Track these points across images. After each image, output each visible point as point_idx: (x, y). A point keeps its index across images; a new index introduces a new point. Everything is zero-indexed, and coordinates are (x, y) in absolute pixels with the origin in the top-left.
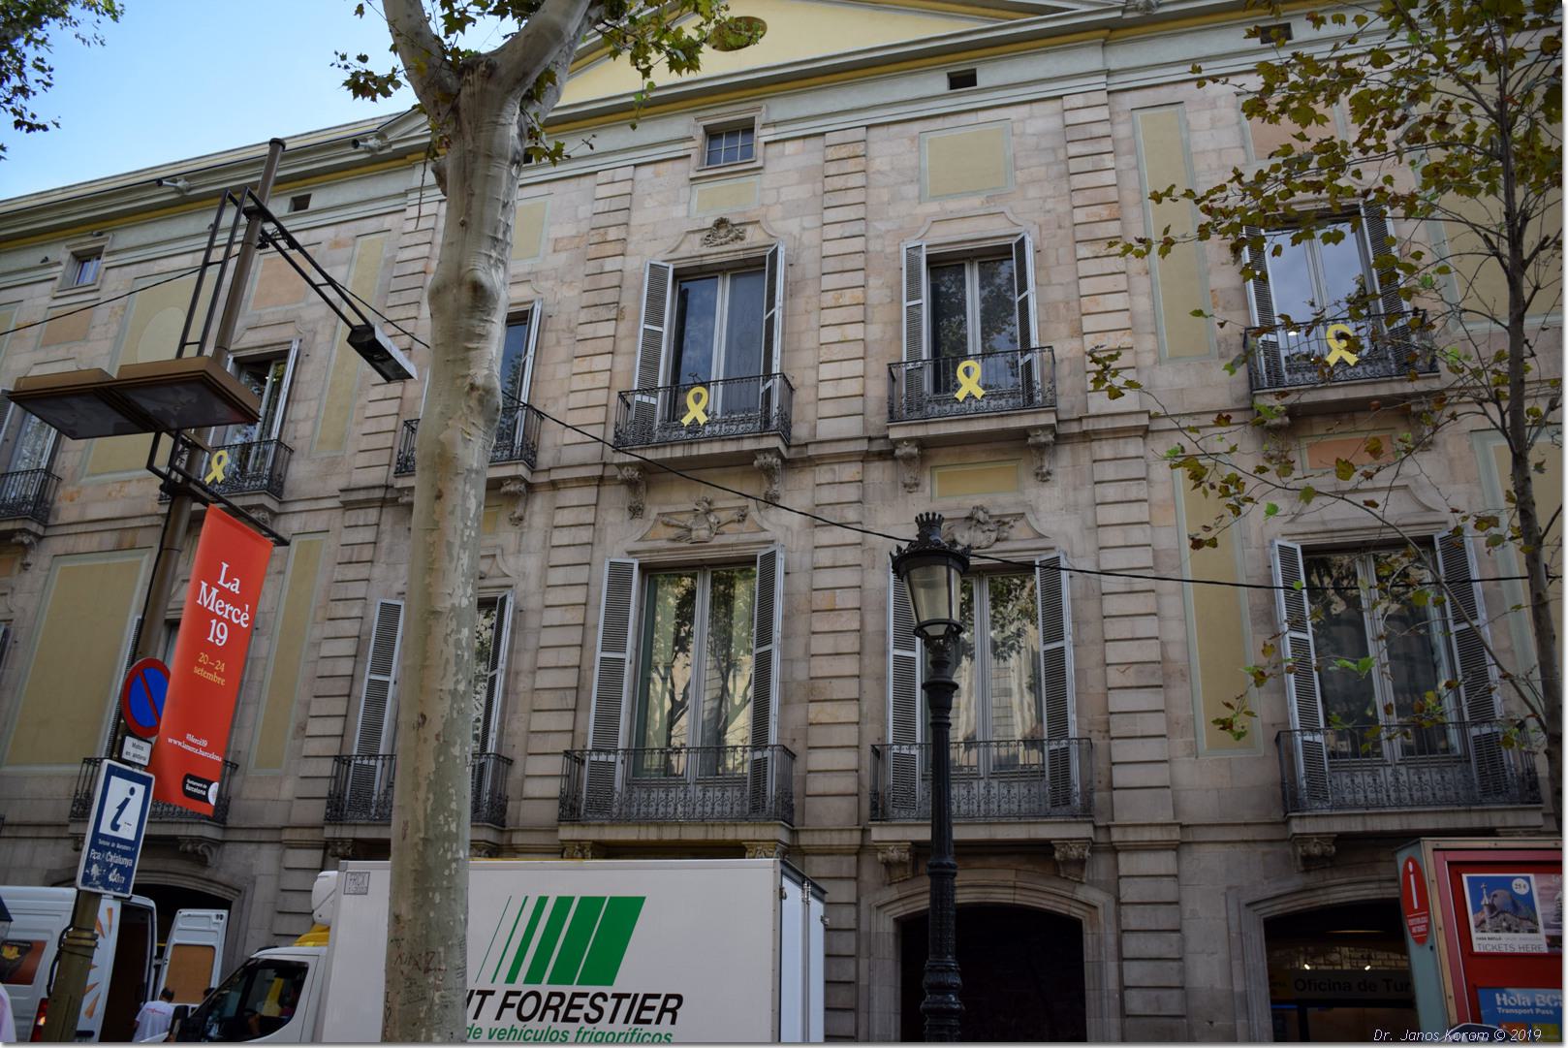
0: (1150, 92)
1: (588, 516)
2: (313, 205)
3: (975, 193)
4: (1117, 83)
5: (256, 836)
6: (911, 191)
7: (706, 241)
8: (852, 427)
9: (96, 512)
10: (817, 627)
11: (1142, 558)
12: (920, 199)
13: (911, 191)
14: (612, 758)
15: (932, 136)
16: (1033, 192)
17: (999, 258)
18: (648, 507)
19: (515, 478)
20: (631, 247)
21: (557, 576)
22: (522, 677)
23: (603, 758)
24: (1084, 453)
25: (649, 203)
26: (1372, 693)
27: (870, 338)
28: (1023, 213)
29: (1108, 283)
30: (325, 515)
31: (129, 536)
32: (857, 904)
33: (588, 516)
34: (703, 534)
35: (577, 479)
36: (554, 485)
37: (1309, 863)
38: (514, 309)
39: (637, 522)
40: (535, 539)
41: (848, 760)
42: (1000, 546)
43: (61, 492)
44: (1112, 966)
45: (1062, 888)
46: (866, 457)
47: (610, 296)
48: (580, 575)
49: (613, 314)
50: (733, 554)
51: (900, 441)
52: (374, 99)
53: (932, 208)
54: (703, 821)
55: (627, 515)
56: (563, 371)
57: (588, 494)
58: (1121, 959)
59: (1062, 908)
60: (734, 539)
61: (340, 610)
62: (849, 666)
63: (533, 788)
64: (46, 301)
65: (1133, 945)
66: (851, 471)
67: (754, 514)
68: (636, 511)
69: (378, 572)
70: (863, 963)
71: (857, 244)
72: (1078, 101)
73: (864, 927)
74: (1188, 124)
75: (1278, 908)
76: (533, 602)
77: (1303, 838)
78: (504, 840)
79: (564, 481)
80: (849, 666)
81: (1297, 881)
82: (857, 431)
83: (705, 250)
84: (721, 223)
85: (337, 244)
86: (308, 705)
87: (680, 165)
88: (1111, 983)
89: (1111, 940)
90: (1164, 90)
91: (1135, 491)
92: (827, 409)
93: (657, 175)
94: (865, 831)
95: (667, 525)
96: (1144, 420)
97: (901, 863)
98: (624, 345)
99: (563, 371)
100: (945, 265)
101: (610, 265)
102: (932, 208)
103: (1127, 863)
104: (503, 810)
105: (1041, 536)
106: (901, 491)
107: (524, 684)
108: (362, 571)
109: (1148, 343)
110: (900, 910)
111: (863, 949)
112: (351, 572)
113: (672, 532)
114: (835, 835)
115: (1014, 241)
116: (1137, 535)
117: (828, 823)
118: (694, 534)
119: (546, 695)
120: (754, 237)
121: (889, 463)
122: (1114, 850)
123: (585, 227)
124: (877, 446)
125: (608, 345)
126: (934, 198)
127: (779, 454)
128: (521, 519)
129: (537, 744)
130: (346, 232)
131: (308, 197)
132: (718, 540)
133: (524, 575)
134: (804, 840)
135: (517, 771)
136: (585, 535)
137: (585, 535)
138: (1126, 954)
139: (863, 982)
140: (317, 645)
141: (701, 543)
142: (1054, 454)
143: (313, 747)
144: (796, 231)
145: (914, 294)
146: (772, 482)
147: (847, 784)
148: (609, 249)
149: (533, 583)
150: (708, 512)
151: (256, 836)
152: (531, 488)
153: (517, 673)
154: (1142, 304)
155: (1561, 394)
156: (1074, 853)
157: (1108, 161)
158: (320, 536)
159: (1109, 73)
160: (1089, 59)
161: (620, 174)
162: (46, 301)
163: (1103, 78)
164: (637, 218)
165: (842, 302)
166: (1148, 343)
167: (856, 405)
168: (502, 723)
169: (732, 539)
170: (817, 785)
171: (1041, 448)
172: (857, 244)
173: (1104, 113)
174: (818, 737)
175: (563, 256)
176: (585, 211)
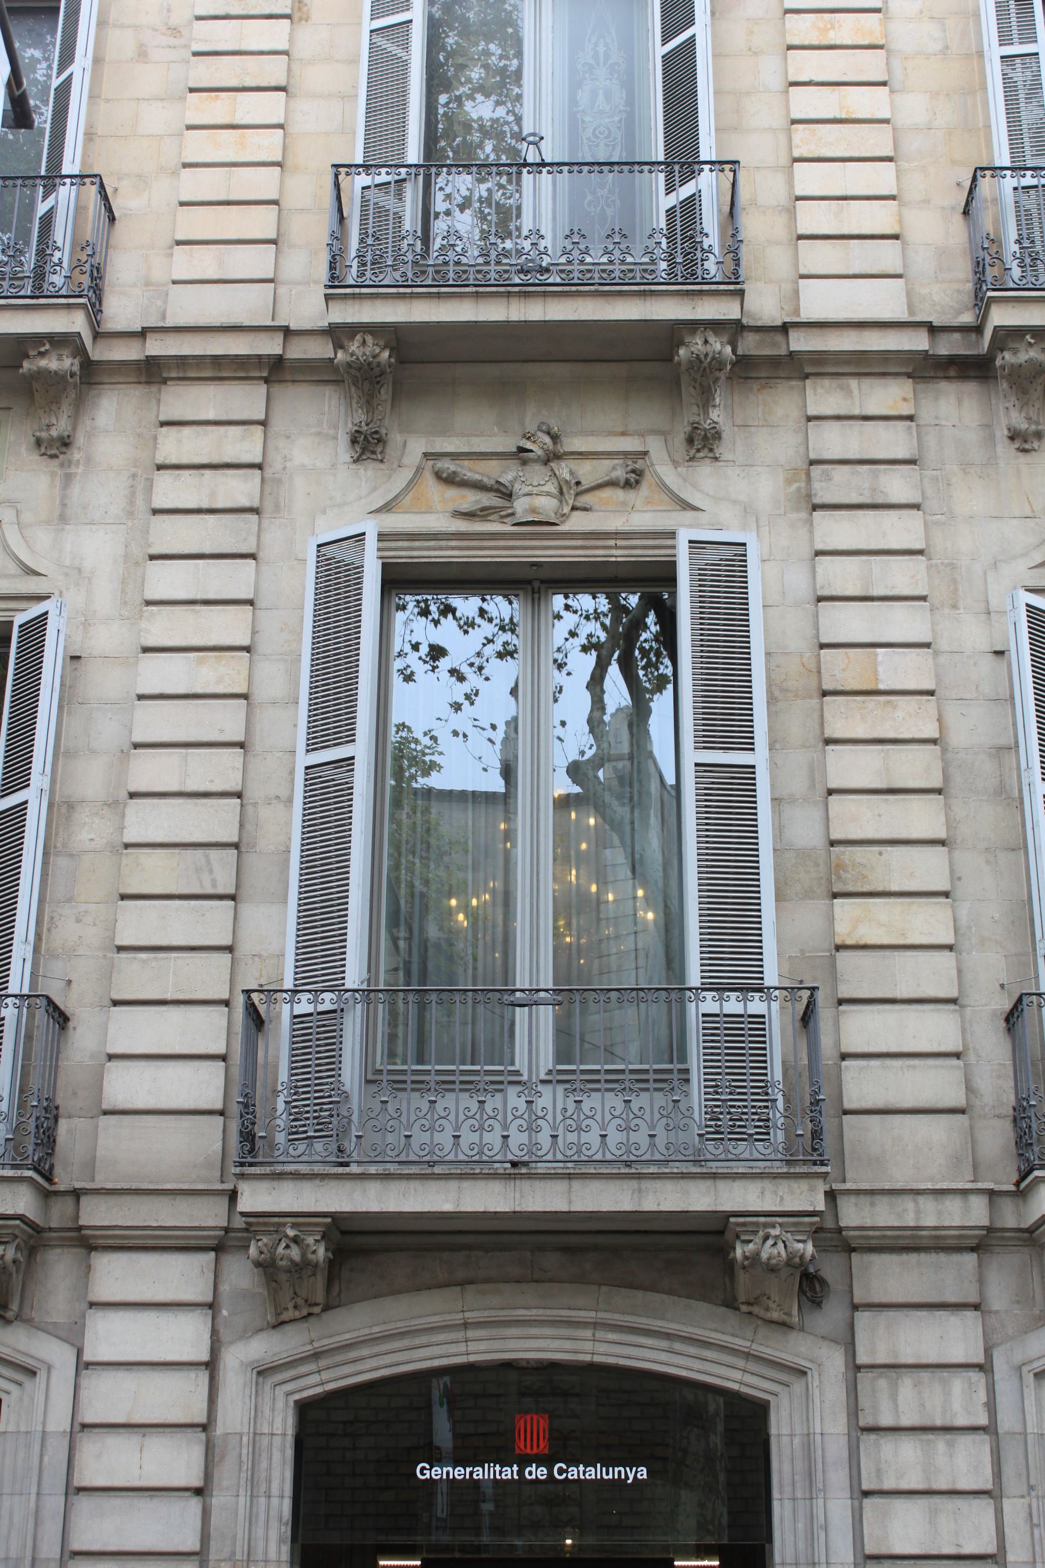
1: (245, 446)
10: (837, 729)
14: (756, 1006)
18: (396, 438)
19: (59, 341)
22: (82, 815)
23: (733, 1005)
24: (782, 404)
26: (303, 925)
27: (903, 119)
32: (211, 1365)
33: (245, 446)
34: (547, 505)
35: (217, 361)
36: (153, 372)
39: (369, 471)
44: (838, 1507)
46: (925, 369)
50: (618, 555)
51: (1017, 333)
55: (344, 452)
56: (158, 118)
60: (619, 520)
65: (177, 1462)
66: (888, 395)
67: (664, 469)
68: (367, 445)
70: (1013, 1508)
73: (1007, 1421)
76: (108, 638)
78: (58, 1215)
79: (182, 361)
82: (896, 311)
89: (836, 1448)
94: (233, 1196)
95: (450, 480)
97: (302, 1268)
98: (315, 78)
99: (158, 118)
103: (116, 1275)
104: (48, 1140)
106: (1005, 449)
107: (90, 832)
111: (1009, 1471)
113: (470, 499)
114: (928, 1204)
117: (900, 1177)
118: (520, 505)
121: (970, 388)
124: (947, 347)
127: (80, 351)
128: (65, 443)
129: (138, 977)
132: (578, 522)
133: (78, 573)
134: (853, 1215)
135: (84, 1041)
136: (239, 489)
137: (239, 489)
141: (539, 526)
142: (79, 406)
146: (706, 401)
149: (104, 595)
150: (551, 457)
152: (92, 374)
153: (71, 806)
170: (125, 1086)
171: (705, 378)
174: (858, 975)
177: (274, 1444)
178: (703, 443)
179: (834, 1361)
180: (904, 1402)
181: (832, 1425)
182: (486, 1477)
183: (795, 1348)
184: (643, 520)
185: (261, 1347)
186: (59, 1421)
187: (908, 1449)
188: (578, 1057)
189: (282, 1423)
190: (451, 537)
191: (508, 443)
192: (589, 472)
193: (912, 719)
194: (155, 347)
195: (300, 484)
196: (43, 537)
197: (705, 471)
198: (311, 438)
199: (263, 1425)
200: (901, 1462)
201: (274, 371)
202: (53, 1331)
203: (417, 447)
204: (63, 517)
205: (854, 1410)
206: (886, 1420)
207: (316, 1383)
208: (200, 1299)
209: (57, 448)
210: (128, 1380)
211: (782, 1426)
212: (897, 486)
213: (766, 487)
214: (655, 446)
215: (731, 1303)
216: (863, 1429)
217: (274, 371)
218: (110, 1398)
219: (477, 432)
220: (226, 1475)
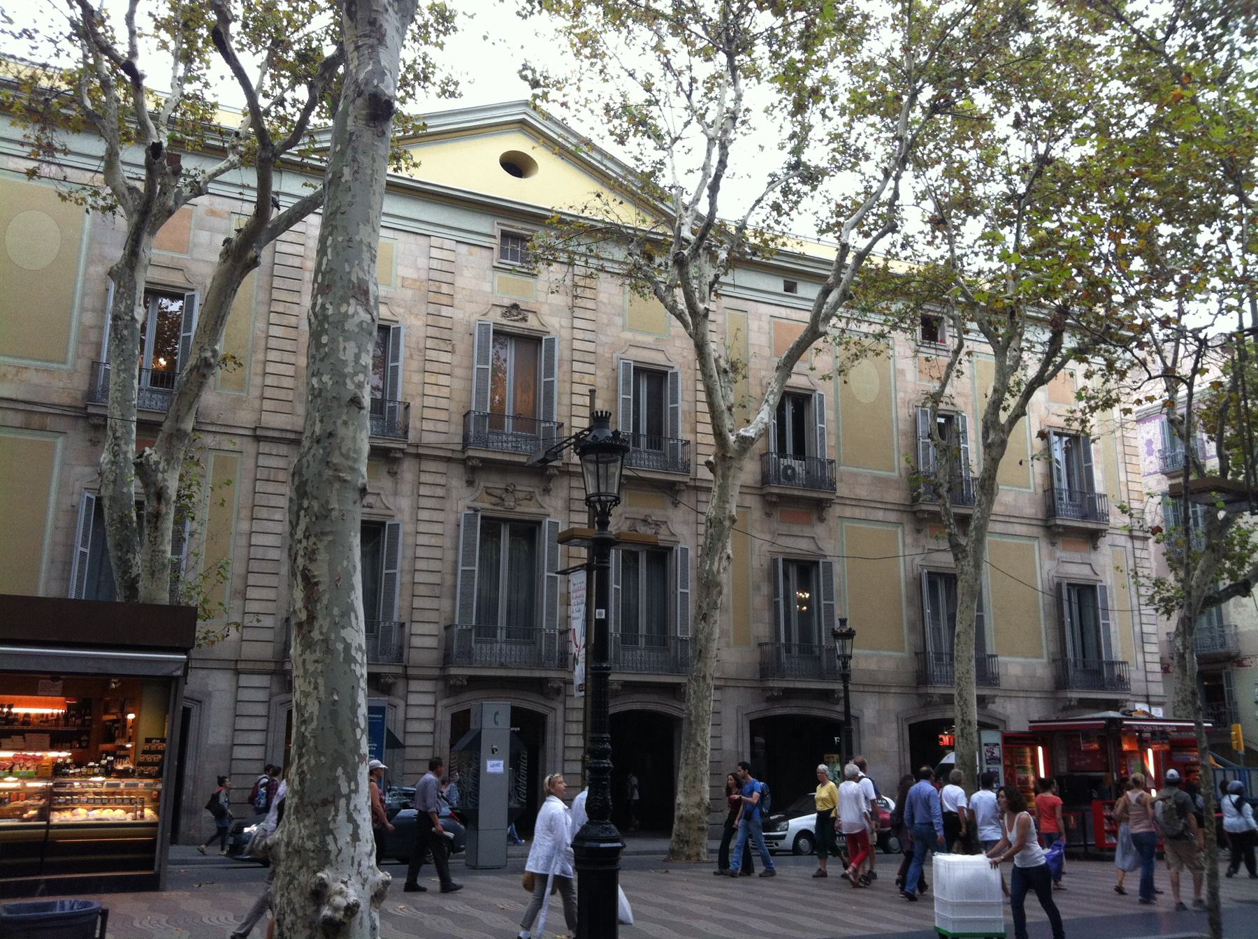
3: (650, 333)
5: (210, 664)
6: (619, 321)
7: (504, 315)
12: (624, 328)
13: (619, 321)
16: (678, 343)
24: (565, 482)
25: (466, 273)
30: (237, 440)
31: (36, 420)
32: (435, 706)
37: (769, 699)
39: (471, 489)
40: (406, 488)
44: (560, 738)
45: (677, 704)
52: (731, 141)
53: (628, 335)
54: (502, 666)
60: (528, 510)
61: (264, 513)
68: (470, 483)
75: (754, 717)
77: (772, 689)
81: (763, 706)
83: (504, 322)
84: (515, 306)
87: (485, 253)
89: (560, 725)
93: (471, 254)
101: (445, 311)
102: (628, 335)
103: (414, 685)
105: (673, 535)
113: (494, 500)
119: (422, 587)
120: (532, 323)
122: (407, 678)
123: (424, 276)
126: (631, 330)
132: (518, 509)
133: (400, 510)
136: (440, 492)
137: (440, 492)
141: (511, 510)
144: (557, 326)
148: (445, 300)
151: (210, 664)
155: (52, 468)
156: (555, 685)
158: (235, 455)
169: (526, 510)
174: (417, 616)
175: (409, 293)
176: (423, 262)
178: (547, 491)
179: (561, 707)
181: (560, 720)
182: (385, 221)
183: (554, 704)
184: (533, 510)
185: (445, 702)
188: (993, 850)
189: (449, 718)
191: (502, 486)
192: (521, 495)
194: (421, 451)
195: (454, 491)
196: (391, 499)
197: (547, 498)
198: (456, 482)
199: (445, 718)
201: (448, 460)
202: (400, 697)
204: (395, 494)
207: (456, 709)
209: (393, 474)
210: (418, 709)
211: (550, 719)
213: (559, 503)
214: (536, 491)
215: (542, 694)
216: (566, 721)
217: (448, 460)
218: (413, 713)
219: (496, 482)
220: (438, 730)
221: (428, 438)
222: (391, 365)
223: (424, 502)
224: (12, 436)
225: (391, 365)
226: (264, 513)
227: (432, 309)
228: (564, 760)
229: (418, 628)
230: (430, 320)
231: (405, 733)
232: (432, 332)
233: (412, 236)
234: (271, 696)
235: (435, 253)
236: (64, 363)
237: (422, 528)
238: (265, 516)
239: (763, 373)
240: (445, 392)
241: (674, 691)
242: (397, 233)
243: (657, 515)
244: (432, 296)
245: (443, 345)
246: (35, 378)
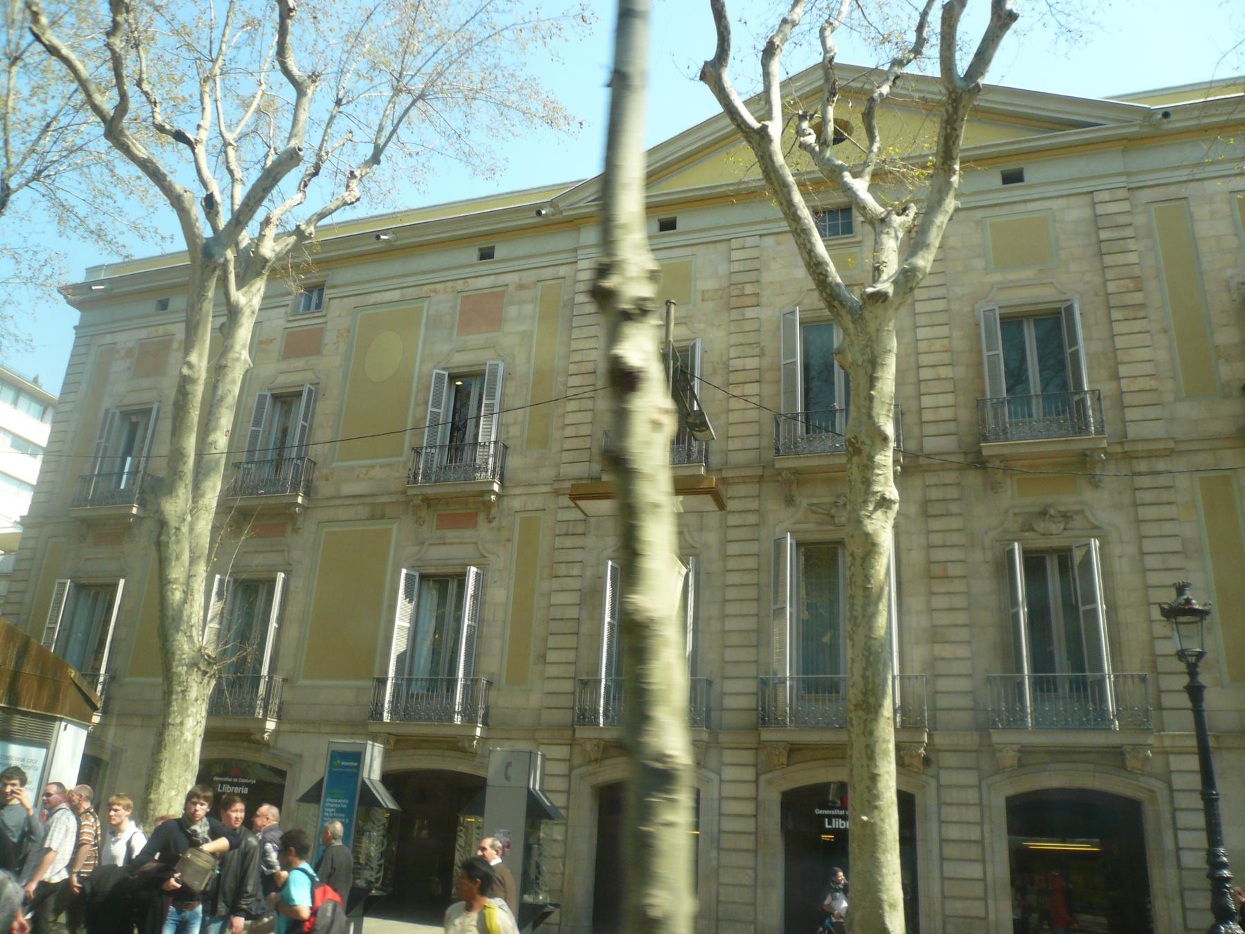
0: (1161, 189)
1: (752, 505)
2: (170, 308)
4: (1135, 181)
6: (979, 263)
8: (949, 443)
9: (349, 489)
11: (1174, 545)
12: (987, 270)
13: (979, 263)
15: (993, 220)
16: (1073, 267)
17: (1053, 324)
20: (764, 300)
21: (733, 549)
28: (1068, 280)
29: (1137, 340)
33: (752, 505)
38: (1004, 311)
41: (964, 685)
42: (1066, 533)
43: (317, 473)
44: (934, 825)
47: (751, 338)
48: (753, 548)
49: (756, 351)
53: (996, 277)
57: (752, 489)
58: (1176, 829)
59: (1129, 793)
61: (562, 570)
62: (961, 618)
63: (729, 702)
64: (282, 323)
69: (589, 541)
71: (941, 305)
72: (1106, 196)
73: (985, 802)
74: (1191, 216)
80: (961, 618)
85: (521, 287)
86: (546, 640)
88: (1169, 844)
89: (1167, 816)
90: (1172, 188)
91: (1165, 496)
92: (930, 429)
93: (778, 244)
95: (815, 513)
96: (1172, 445)
100: (1011, 323)
101: (750, 313)
102: (996, 277)
108: (579, 541)
109: (1169, 385)
110: (1010, 790)
112: (569, 542)
115: (1063, 306)
116: (1168, 528)
118: (837, 520)
125: (755, 376)
130: (528, 277)
131: (493, 248)
136: (752, 518)
137: (752, 518)
138: (1179, 826)
139: (987, 841)
140: (549, 595)
143: (552, 671)
145: (437, 404)
147: (965, 701)
148: (749, 301)
154: (1162, 355)
157: (1132, 244)
159: (1129, 174)
160: (1113, 162)
161: (749, 242)
162: (282, 323)
163: (1124, 178)
164: (766, 277)
165: (933, 348)
166: (1169, 385)
167: (951, 427)
168: (155, 426)
172: (941, 305)
173: (1125, 206)
176: (723, 269)
177: (202, 595)
180: (949, 796)
181: (932, 802)
186: (716, 796)
187: (955, 810)
190: (1050, 126)
193: (959, 586)
200: (952, 813)
203: (805, 502)
204: (701, 529)
205: (939, 798)
206: (949, 801)
208: (562, 773)
211: (918, 801)
212: (954, 508)
216: (940, 804)
221: (735, 458)
222: (1069, 351)
223: (733, 534)
224: (360, 528)
225: (1069, 351)
226: (562, 570)
227: (735, 314)
228: (943, 859)
229: (730, 686)
230: (733, 328)
231: (720, 815)
232: (734, 339)
233: (711, 246)
234: (571, 769)
235: (736, 255)
236: (401, 455)
237: (731, 564)
238: (564, 573)
239: (1229, 272)
240: (1148, 368)
241: (837, 753)
242: (695, 249)
243: (1067, 501)
244: (734, 302)
245: (749, 351)
246: (377, 473)
